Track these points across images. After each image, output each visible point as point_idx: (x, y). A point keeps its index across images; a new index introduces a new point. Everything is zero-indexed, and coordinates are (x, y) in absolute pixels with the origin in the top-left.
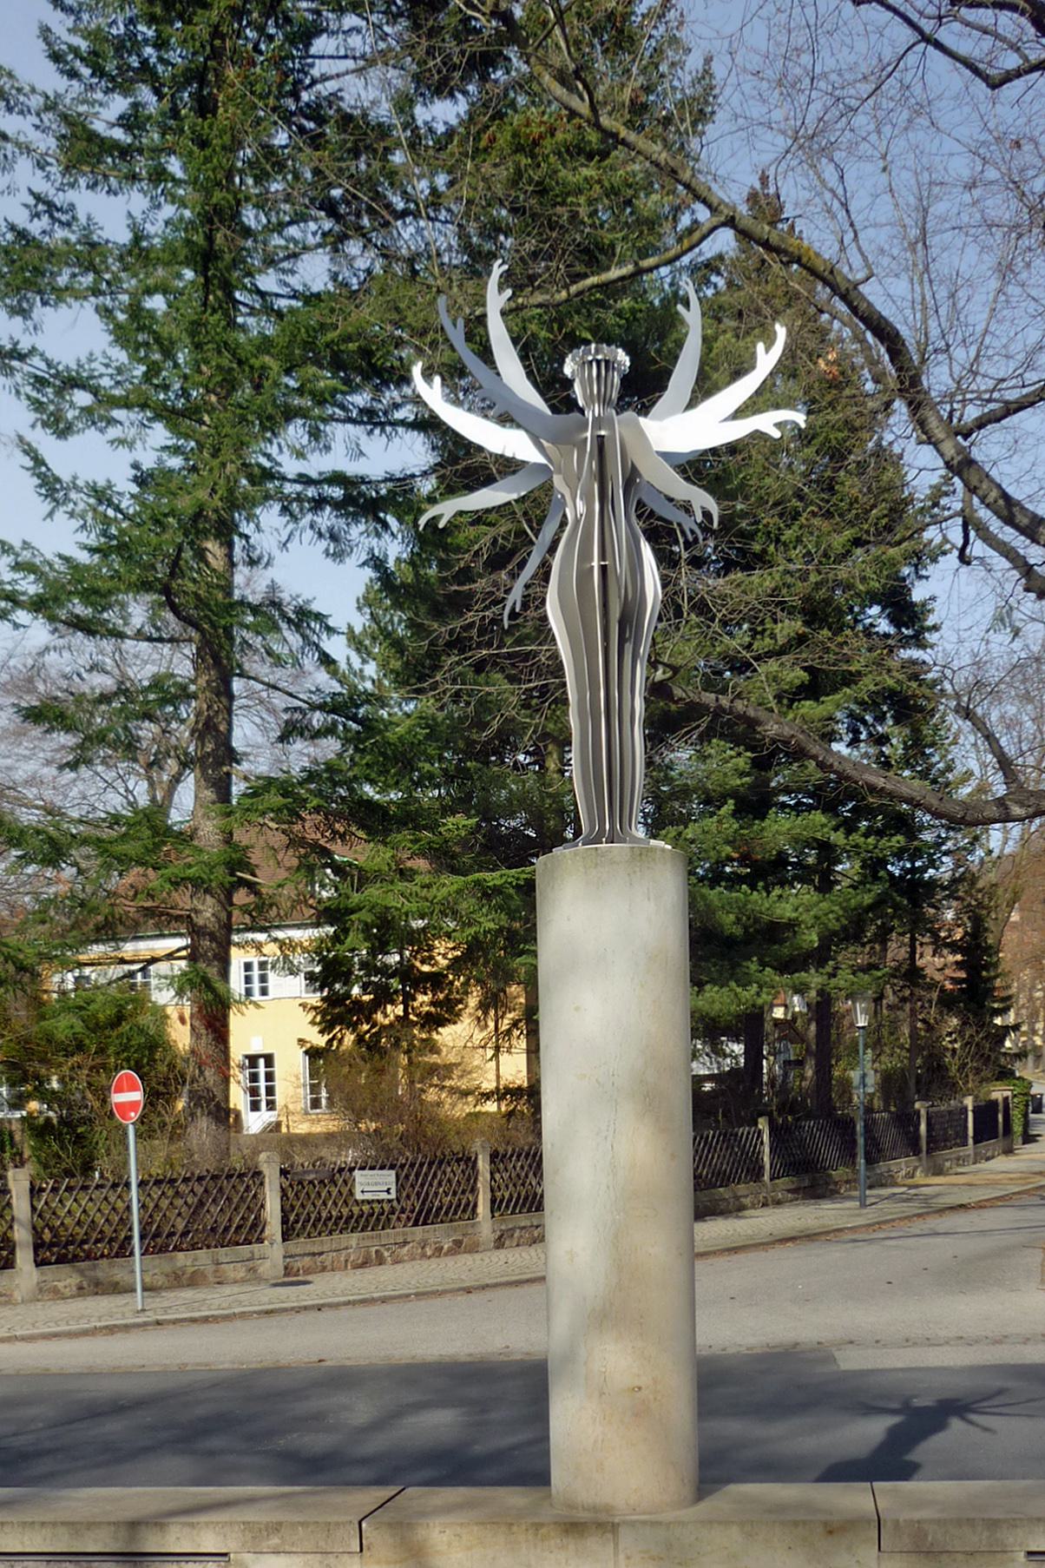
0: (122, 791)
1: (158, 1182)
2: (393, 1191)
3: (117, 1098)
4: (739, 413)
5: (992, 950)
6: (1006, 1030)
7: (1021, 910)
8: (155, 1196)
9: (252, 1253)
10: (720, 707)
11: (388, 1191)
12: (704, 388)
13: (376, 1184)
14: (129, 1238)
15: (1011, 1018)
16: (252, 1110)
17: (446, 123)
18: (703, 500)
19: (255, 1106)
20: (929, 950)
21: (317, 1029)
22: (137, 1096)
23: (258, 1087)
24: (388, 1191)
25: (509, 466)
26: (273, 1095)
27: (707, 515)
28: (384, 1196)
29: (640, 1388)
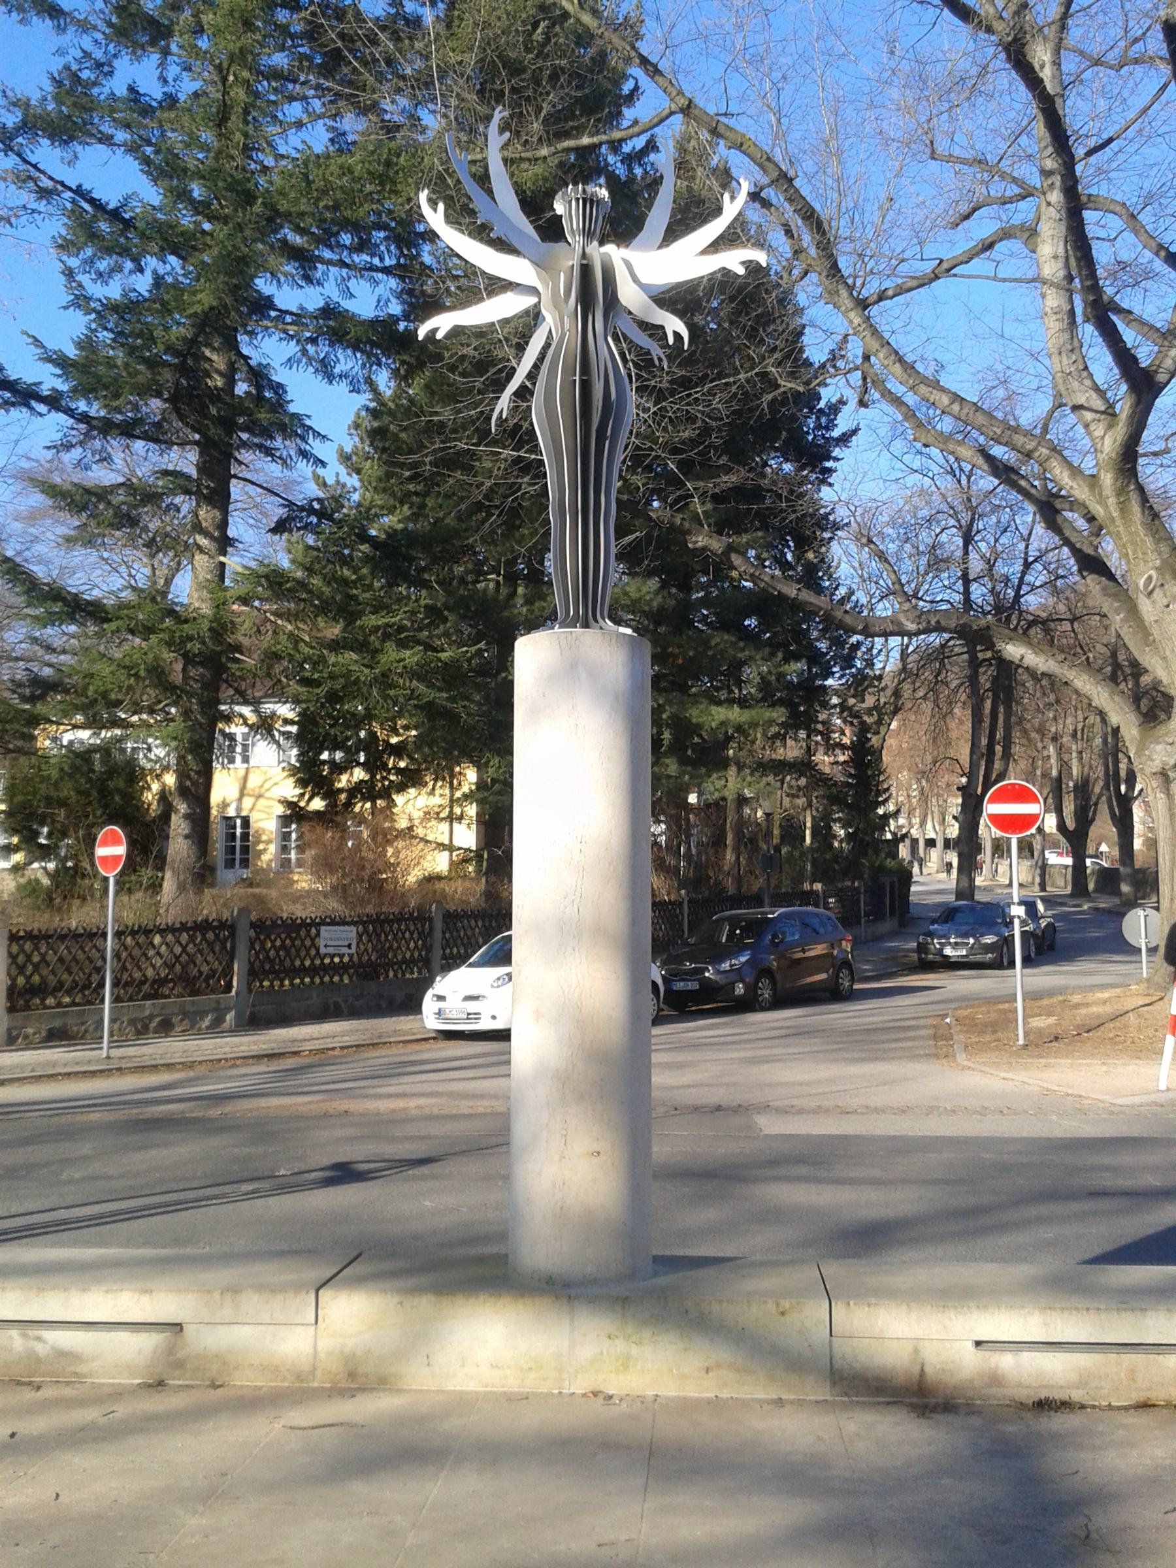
0: (125, 575)
1: (133, 933)
2: (354, 946)
3: (101, 851)
4: (716, 246)
5: (877, 753)
6: (886, 817)
7: (899, 721)
8: (87, 971)
9: (218, 1002)
10: (672, 524)
11: (349, 946)
12: (675, 231)
13: (338, 939)
14: (102, 985)
15: (891, 807)
16: (226, 867)
17: (297, 881)
18: (674, 325)
19: (230, 864)
20: (821, 750)
21: (136, 63)
22: (121, 850)
23: (234, 847)
24: (349, 946)
25: (498, 286)
26: (248, 853)
27: (677, 335)
28: (345, 950)
29: (598, 1153)
